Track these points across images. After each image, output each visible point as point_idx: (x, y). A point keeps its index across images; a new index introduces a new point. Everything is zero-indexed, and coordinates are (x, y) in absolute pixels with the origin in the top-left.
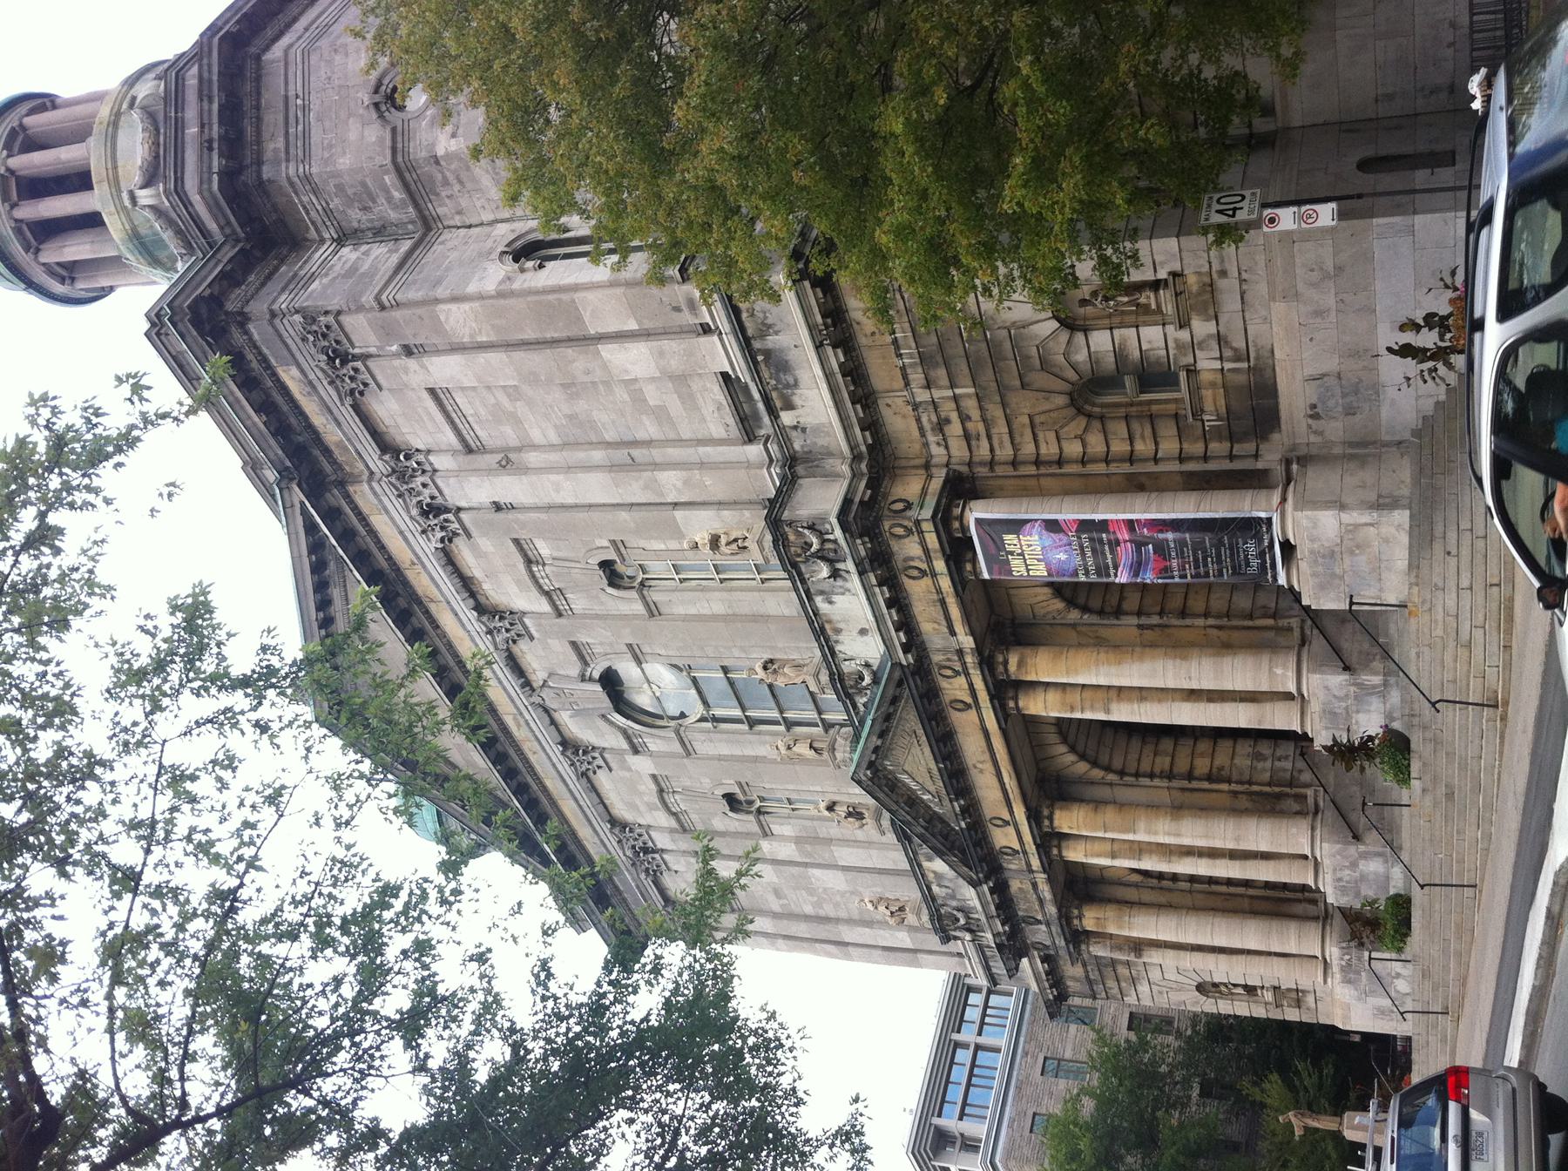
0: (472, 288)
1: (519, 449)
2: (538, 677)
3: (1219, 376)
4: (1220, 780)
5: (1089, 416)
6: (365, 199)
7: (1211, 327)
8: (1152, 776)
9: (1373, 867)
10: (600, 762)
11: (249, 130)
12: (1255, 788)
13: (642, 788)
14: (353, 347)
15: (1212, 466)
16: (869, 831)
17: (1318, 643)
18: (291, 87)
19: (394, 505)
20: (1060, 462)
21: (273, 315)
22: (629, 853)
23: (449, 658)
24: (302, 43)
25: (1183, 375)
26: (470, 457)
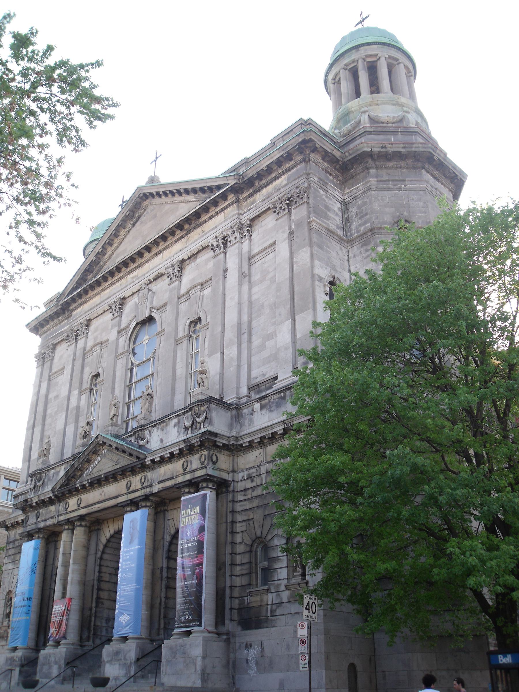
0: (317, 263)
1: (250, 281)
2: (153, 287)
3: (265, 603)
4: (97, 602)
5: (252, 546)
6: (361, 215)
7: (285, 600)
8: (100, 572)
9: (55, 672)
10: (116, 315)
11: (391, 164)
12: (93, 618)
13: (104, 334)
14: (295, 208)
15: (227, 600)
16: (80, 442)
17: (149, 647)
18: (409, 182)
19: (227, 224)
20: (233, 532)
21: (308, 174)
22: (76, 328)
23: (163, 247)
24: (428, 187)
25: (266, 587)
26: (247, 259)
